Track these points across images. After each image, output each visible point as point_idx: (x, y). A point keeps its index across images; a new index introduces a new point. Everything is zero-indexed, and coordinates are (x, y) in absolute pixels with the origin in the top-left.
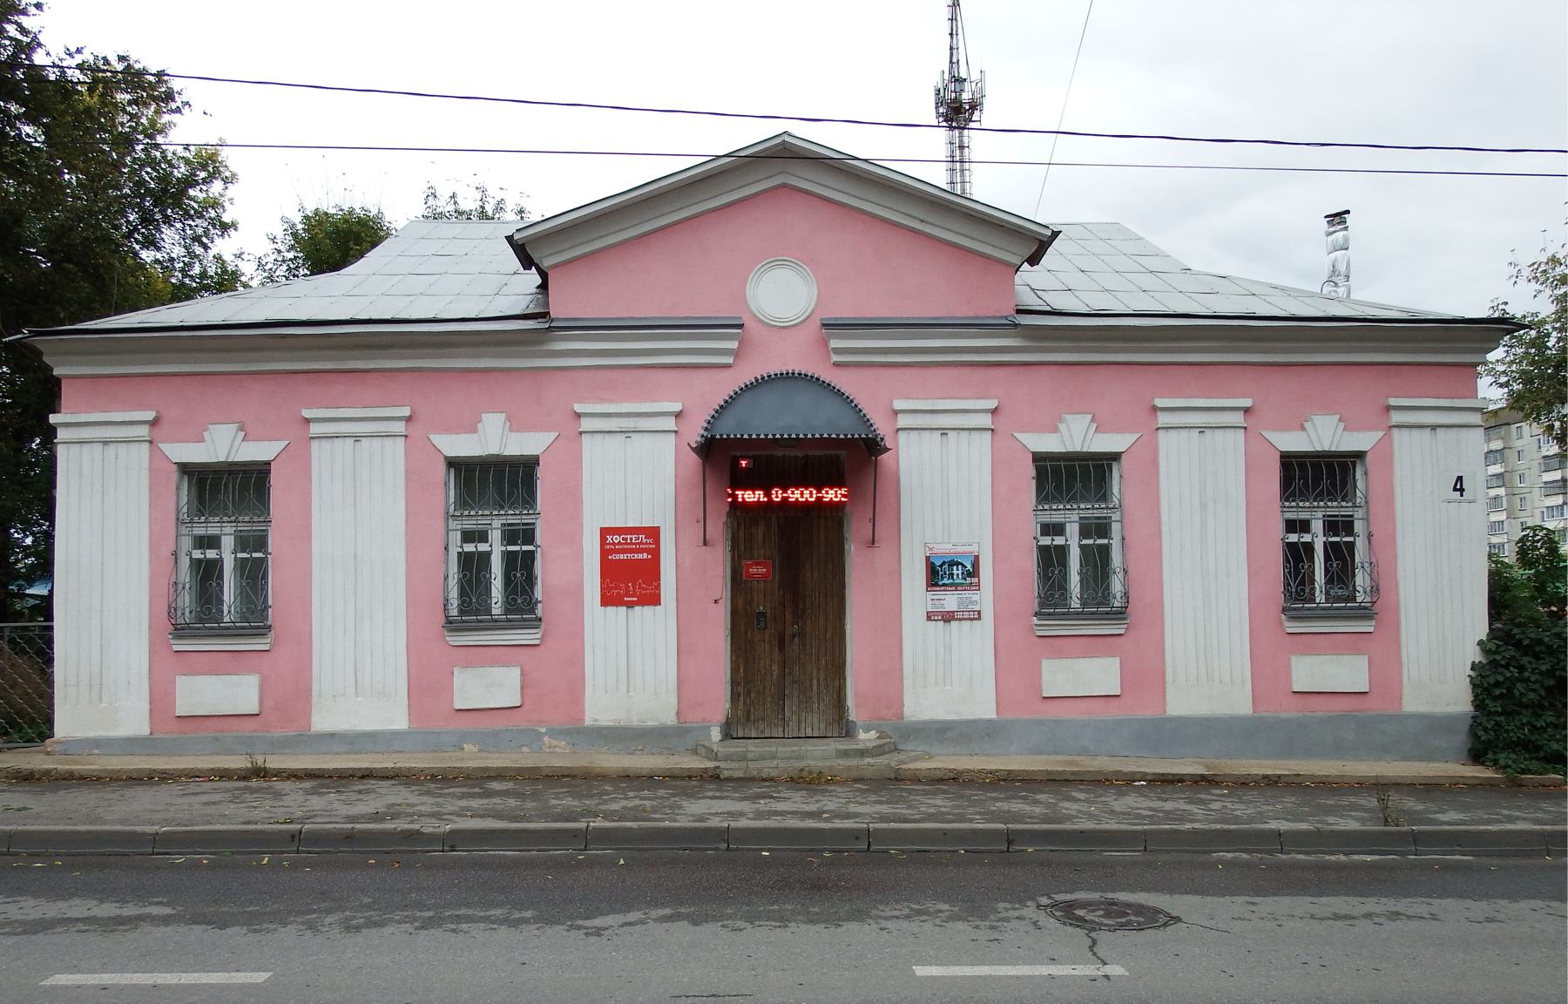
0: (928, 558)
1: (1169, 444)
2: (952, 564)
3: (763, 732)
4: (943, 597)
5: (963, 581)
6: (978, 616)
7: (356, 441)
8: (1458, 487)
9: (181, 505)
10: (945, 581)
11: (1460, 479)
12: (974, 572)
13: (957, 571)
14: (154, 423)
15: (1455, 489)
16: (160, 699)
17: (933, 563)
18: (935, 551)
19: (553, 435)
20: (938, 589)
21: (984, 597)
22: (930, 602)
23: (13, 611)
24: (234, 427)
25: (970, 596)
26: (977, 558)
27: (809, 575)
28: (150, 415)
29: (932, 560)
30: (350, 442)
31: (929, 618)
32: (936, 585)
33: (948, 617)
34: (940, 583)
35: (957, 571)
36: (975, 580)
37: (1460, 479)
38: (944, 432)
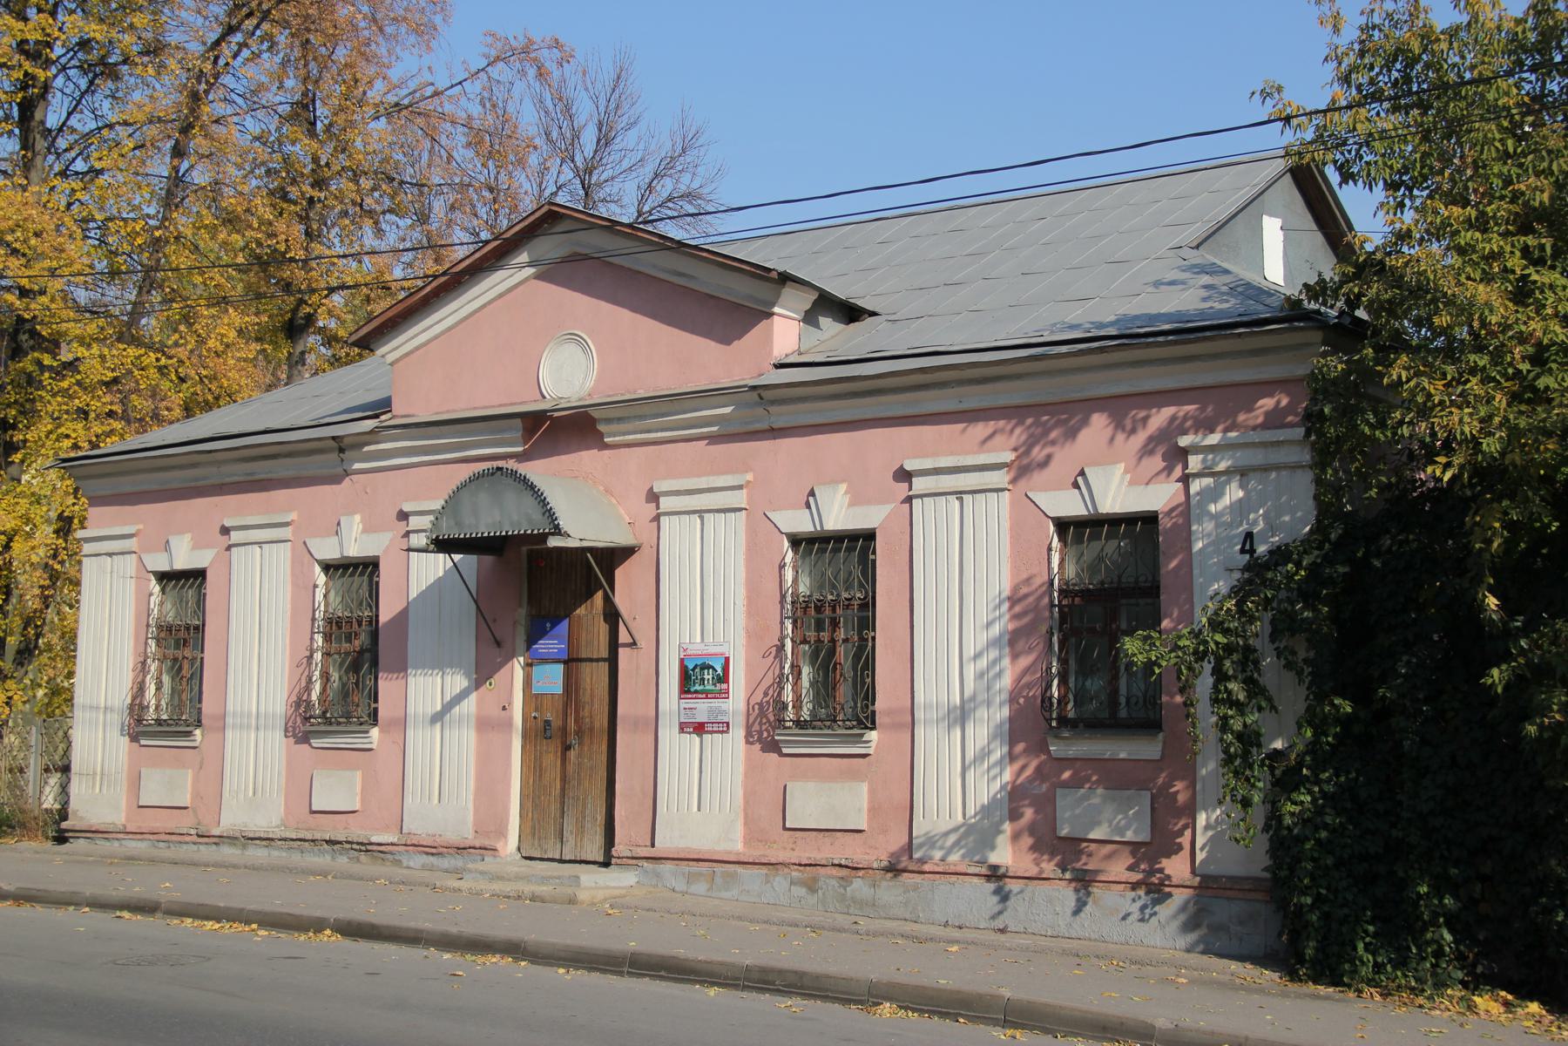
0: (682, 661)
6: (725, 728)
8: (1247, 547)
9: (152, 606)
10: (697, 687)
12: (724, 678)
13: (708, 676)
15: (1243, 551)
17: (686, 667)
18: (689, 652)
22: (683, 711)
23: (1379, 925)
25: (717, 705)
26: (727, 660)
27: (588, 680)
31: (682, 730)
32: (689, 692)
34: (692, 690)
35: (708, 676)
36: (724, 686)
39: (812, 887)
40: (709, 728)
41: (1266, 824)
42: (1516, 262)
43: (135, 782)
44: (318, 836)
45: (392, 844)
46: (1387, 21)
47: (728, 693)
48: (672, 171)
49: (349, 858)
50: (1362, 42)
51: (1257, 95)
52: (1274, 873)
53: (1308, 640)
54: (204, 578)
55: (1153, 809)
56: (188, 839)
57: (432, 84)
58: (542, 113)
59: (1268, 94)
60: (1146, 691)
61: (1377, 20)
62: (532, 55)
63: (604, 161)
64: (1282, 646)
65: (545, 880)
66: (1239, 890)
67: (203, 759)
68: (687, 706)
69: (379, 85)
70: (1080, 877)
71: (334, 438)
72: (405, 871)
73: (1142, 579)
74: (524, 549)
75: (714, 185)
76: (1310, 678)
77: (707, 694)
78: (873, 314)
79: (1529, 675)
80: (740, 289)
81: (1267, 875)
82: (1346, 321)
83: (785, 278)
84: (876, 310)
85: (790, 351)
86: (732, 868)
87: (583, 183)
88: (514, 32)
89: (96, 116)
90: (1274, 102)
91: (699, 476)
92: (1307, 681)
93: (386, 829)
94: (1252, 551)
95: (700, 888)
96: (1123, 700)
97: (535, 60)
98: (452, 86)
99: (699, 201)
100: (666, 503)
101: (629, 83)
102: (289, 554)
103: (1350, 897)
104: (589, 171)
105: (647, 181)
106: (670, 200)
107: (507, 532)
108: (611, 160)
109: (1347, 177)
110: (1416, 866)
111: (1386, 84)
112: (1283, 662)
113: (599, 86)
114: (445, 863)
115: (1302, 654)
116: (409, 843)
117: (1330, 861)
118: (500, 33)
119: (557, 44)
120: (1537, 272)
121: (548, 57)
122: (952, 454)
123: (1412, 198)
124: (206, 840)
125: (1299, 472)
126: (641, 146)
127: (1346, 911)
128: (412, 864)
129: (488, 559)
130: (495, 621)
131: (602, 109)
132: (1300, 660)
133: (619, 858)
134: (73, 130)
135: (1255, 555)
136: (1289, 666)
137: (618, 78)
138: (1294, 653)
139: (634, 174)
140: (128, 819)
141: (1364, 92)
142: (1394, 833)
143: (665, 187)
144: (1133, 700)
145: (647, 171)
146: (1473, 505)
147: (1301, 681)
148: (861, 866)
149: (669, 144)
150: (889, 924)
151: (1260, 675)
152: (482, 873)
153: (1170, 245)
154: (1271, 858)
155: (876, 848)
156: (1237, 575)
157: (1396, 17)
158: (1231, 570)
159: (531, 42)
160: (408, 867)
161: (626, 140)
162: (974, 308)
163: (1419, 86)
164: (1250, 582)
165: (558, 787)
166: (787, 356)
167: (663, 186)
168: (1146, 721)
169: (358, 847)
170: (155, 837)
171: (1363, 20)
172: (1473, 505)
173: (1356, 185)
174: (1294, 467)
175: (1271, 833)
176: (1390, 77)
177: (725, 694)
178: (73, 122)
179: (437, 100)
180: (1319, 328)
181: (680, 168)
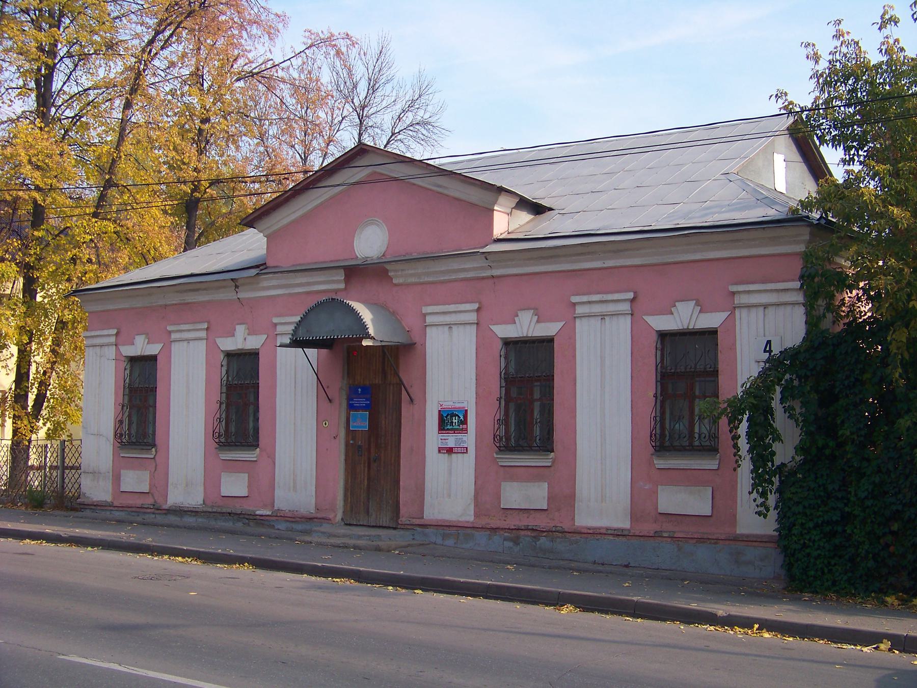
0: (440, 411)
1: (581, 327)
2: (453, 415)
3: (359, 521)
5: (458, 427)
7: (450, 327)
8: (768, 349)
10: (449, 427)
12: (465, 422)
13: (455, 420)
15: (765, 351)
16: (211, 481)
18: (444, 407)
22: (440, 441)
24: (143, 336)
25: (460, 437)
26: (466, 411)
28: (631, 295)
31: (439, 451)
32: (444, 430)
33: (450, 451)
34: (446, 428)
36: (465, 426)
38: (450, 326)
39: (516, 541)
40: (455, 450)
43: (117, 479)
44: (224, 510)
45: (268, 516)
47: (467, 430)
48: (413, 108)
49: (243, 523)
53: (801, 402)
54: (156, 360)
56: (149, 510)
57: (272, 60)
58: (334, 73)
60: (710, 430)
61: (838, 58)
62: (333, 43)
64: (787, 406)
65: (359, 537)
67: (156, 465)
68: (443, 438)
70: (672, 536)
72: (277, 531)
74: (345, 345)
75: (438, 116)
77: (455, 431)
78: (551, 209)
80: (474, 195)
81: (776, 534)
82: (823, 222)
83: (501, 190)
85: (502, 232)
86: (469, 531)
88: (321, 27)
89: (77, 83)
90: (783, 101)
92: (801, 424)
93: (265, 506)
94: (770, 351)
95: (450, 542)
96: (697, 436)
98: (284, 61)
99: (429, 127)
100: (429, 320)
103: (822, 544)
105: (398, 114)
106: (411, 126)
107: (337, 336)
110: (858, 527)
111: (844, 91)
112: (787, 414)
113: (368, 57)
114: (299, 527)
117: (811, 525)
121: (342, 45)
124: (160, 511)
125: (797, 306)
126: (394, 94)
127: (819, 552)
128: (279, 527)
130: (328, 387)
131: (370, 71)
134: (65, 93)
135: (772, 354)
137: (381, 53)
139: (389, 110)
140: (114, 498)
143: (409, 118)
145: (398, 108)
146: (891, 328)
147: (797, 425)
149: (411, 92)
150: (562, 563)
155: (553, 520)
157: (848, 56)
159: (332, 35)
160: (278, 529)
161: (386, 92)
162: (610, 207)
164: (769, 369)
167: (407, 117)
170: (130, 509)
171: (831, 57)
172: (891, 328)
174: (793, 304)
175: (779, 510)
178: (65, 88)
179: (274, 70)
181: (417, 106)
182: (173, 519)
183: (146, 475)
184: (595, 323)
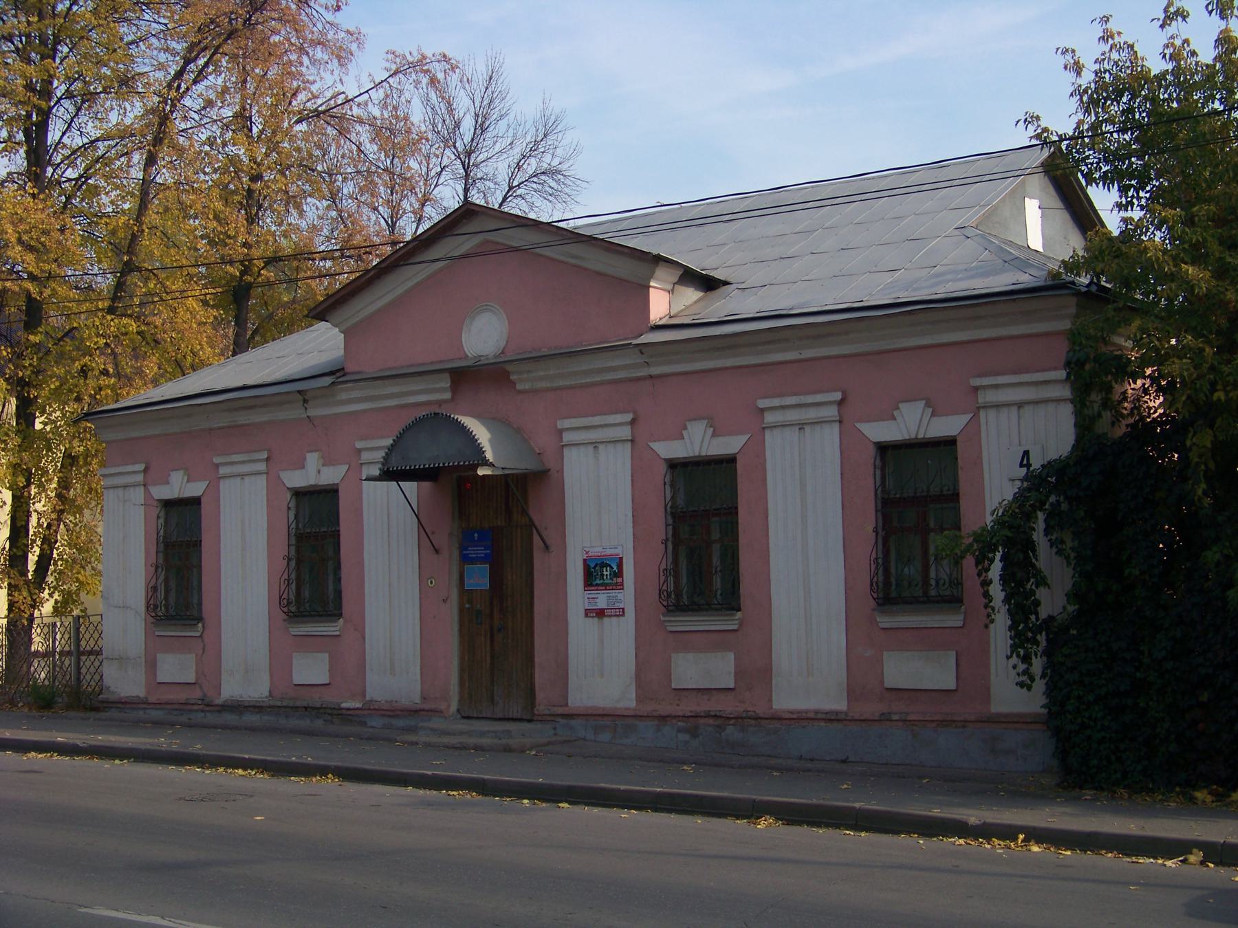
0: (585, 561)
2: (604, 565)
4: (596, 596)
8: (1025, 462)
10: (598, 582)
11: (1026, 453)
12: (619, 573)
13: (606, 572)
14: (841, 403)
15: (1021, 465)
16: (279, 665)
17: (589, 565)
18: (590, 554)
19: (345, 467)
20: (593, 588)
21: (627, 597)
22: (587, 600)
24: (922, 404)
26: (621, 559)
27: (510, 577)
28: (838, 396)
29: (588, 563)
30: (238, 479)
31: (586, 615)
32: (591, 585)
33: (601, 613)
34: (594, 583)
36: (619, 580)
37: (1026, 453)
39: (694, 732)
40: (608, 612)
41: (1043, 672)
42: (1215, 248)
43: (151, 665)
46: (1115, 67)
50: (1096, 83)
51: (1021, 123)
52: (1049, 708)
55: (958, 665)
56: (195, 707)
57: (343, 93)
59: (1029, 122)
60: (951, 574)
62: (425, 68)
63: (480, 146)
65: (482, 734)
66: (1024, 723)
67: (204, 645)
68: (590, 596)
69: (302, 97)
71: (299, 392)
72: (371, 730)
73: (946, 488)
75: (571, 162)
76: (1075, 561)
77: (606, 587)
79: (1232, 554)
80: (622, 268)
81: (1044, 711)
82: (1094, 288)
83: (658, 260)
84: (728, 280)
85: (663, 315)
87: (463, 164)
88: (409, 49)
89: (81, 132)
90: (1034, 128)
91: (593, 416)
94: (1028, 465)
95: (605, 737)
96: (933, 582)
97: (428, 71)
99: (559, 176)
100: (567, 437)
101: (499, 83)
102: (265, 483)
104: (469, 154)
105: (516, 161)
106: (535, 176)
108: (485, 144)
109: (1090, 179)
112: (1054, 550)
114: (401, 723)
115: (1069, 544)
116: (372, 707)
118: (399, 51)
119: (445, 58)
120: (1231, 255)
121: (438, 70)
122: (795, 394)
123: (1139, 198)
129: (426, 485)
131: (478, 104)
132: (1068, 549)
133: (538, 715)
134: (65, 146)
135: (1031, 469)
136: (1059, 552)
137: (490, 79)
138: (1063, 542)
139: (505, 156)
141: (1101, 119)
142: (1138, 675)
143: (531, 166)
144: (941, 582)
145: (516, 153)
146: (1190, 429)
147: (1069, 564)
148: (732, 716)
151: (1037, 560)
152: (432, 730)
153: (955, 226)
154: (1047, 698)
156: (1018, 483)
158: (1013, 480)
159: (424, 57)
160: (372, 727)
162: (806, 278)
163: (1140, 114)
165: (488, 661)
166: (660, 319)
167: (529, 164)
168: (953, 600)
169: (330, 712)
171: (1097, 67)
173: (1097, 186)
174: (1058, 401)
175: (1047, 679)
176: (1119, 108)
177: (620, 586)
178: (66, 140)
180: (1073, 295)
181: (542, 150)
182: (229, 718)
183: (190, 660)
184: (791, 435)
